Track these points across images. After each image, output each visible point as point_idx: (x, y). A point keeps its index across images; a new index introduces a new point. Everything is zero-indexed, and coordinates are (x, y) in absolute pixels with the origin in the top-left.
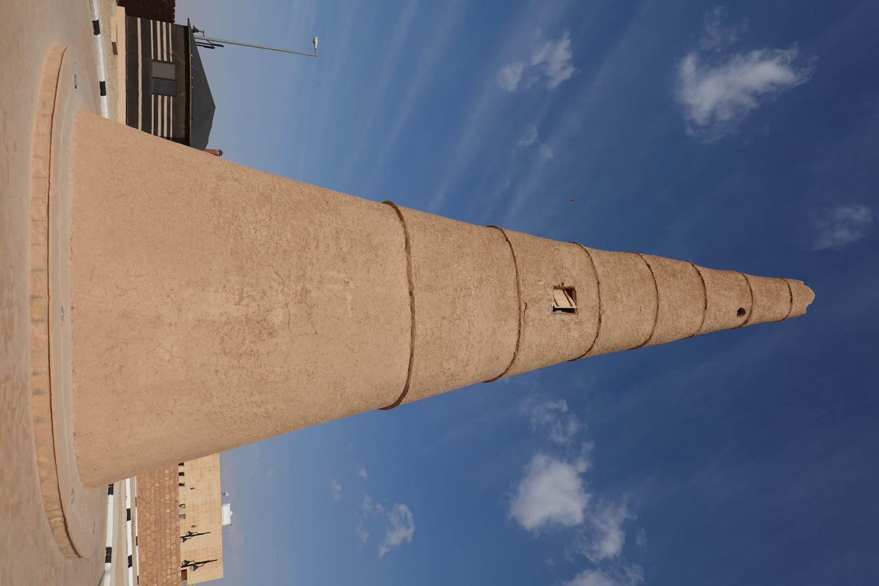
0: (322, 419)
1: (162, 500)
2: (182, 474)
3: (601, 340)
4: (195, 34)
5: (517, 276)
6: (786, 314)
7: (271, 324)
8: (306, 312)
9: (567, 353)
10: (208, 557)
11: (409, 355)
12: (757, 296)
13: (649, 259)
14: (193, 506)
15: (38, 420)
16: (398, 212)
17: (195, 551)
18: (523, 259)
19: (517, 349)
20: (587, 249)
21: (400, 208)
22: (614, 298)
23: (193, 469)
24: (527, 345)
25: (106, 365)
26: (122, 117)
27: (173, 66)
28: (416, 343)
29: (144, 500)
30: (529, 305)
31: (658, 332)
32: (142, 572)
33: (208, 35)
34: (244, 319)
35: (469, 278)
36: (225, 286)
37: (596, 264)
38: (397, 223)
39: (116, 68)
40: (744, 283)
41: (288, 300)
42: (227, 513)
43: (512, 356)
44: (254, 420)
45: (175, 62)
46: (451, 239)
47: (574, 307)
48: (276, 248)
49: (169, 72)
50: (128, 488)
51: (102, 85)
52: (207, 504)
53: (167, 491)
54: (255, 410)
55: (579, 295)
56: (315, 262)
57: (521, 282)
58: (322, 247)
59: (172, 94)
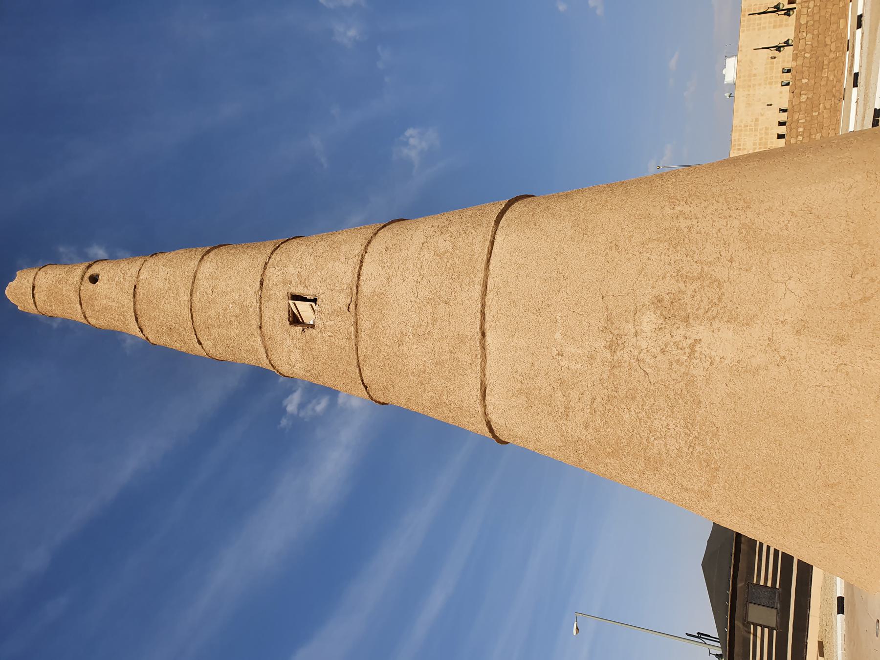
0: (604, 189)
1: (810, 95)
2: (781, 124)
3: (261, 259)
4: (720, 652)
5: (357, 345)
6: (41, 273)
7: (659, 313)
8: (612, 323)
9: (303, 247)
10: (760, 19)
11: (492, 262)
12: (74, 297)
13: (198, 350)
14: (771, 83)
16: (491, 430)
17: (774, 27)
18: (349, 363)
19: (362, 258)
20: (271, 369)
21: (490, 436)
22: (243, 308)
23: (767, 129)
24: (351, 262)
25: (873, 280)
26: (817, 577)
27: (750, 619)
28: (482, 275)
29: (834, 96)
30: (345, 309)
31: (193, 264)
32: (846, 7)
33: (705, 649)
34: (691, 321)
35: (414, 347)
36: (712, 363)
37: (263, 350)
38: (493, 418)
39: (822, 625)
40: (88, 313)
41: (634, 340)
42: (730, 72)
43: (369, 249)
44: (690, 196)
45: (747, 624)
46: (431, 394)
47: (291, 302)
48: (644, 403)
49: (756, 613)
50: (855, 117)
51: (841, 610)
52: (754, 92)
53: (803, 106)
54: (687, 209)
55: (286, 315)
56: (597, 383)
57: (353, 337)
58: (586, 399)
59: (754, 591)
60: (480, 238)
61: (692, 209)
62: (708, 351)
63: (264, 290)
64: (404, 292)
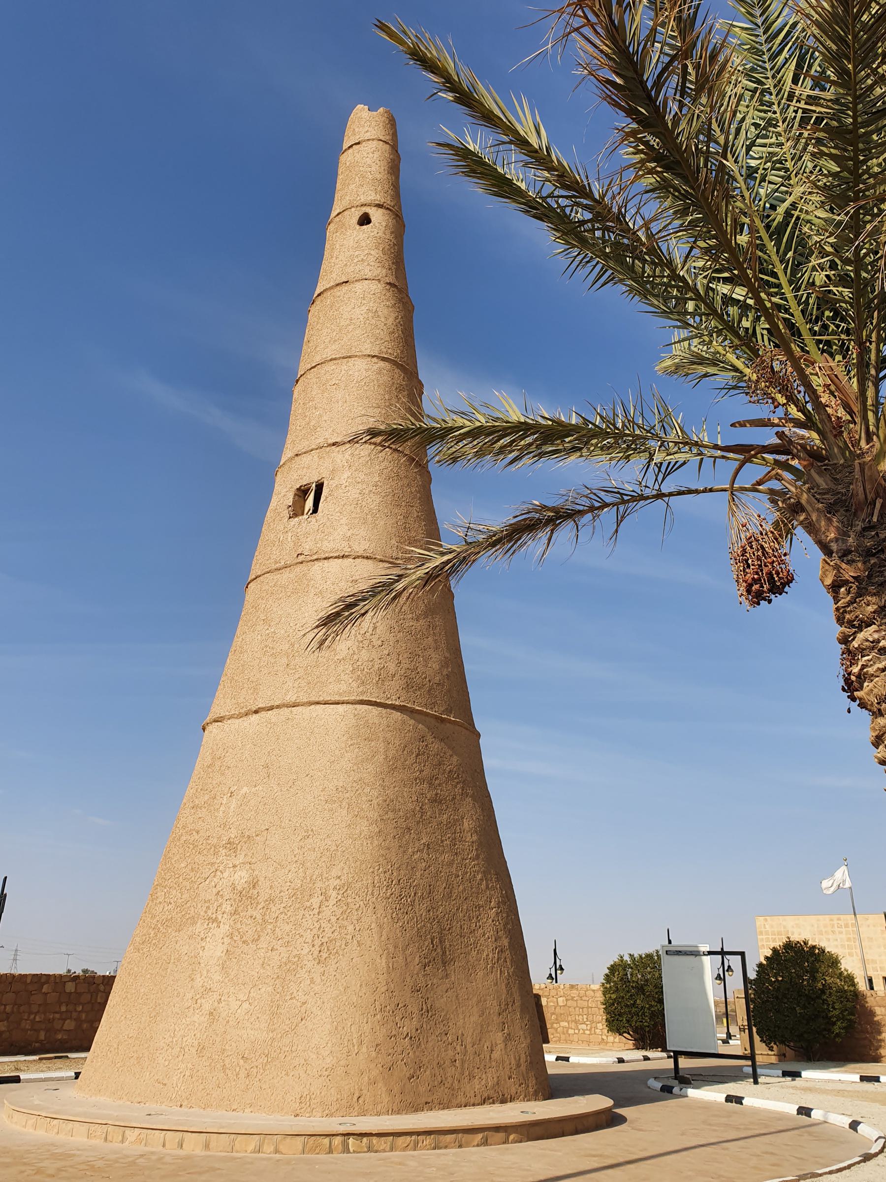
11: (318, 706)
15: (207, 1146)
19: (347, 556)
43: (358, 561)
60: (343, 687)
61: (331, 907)
62: (210, 935)
63: (329, 448)
64: (306, 615)
